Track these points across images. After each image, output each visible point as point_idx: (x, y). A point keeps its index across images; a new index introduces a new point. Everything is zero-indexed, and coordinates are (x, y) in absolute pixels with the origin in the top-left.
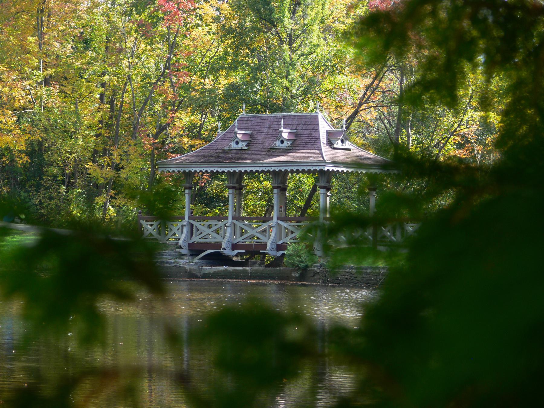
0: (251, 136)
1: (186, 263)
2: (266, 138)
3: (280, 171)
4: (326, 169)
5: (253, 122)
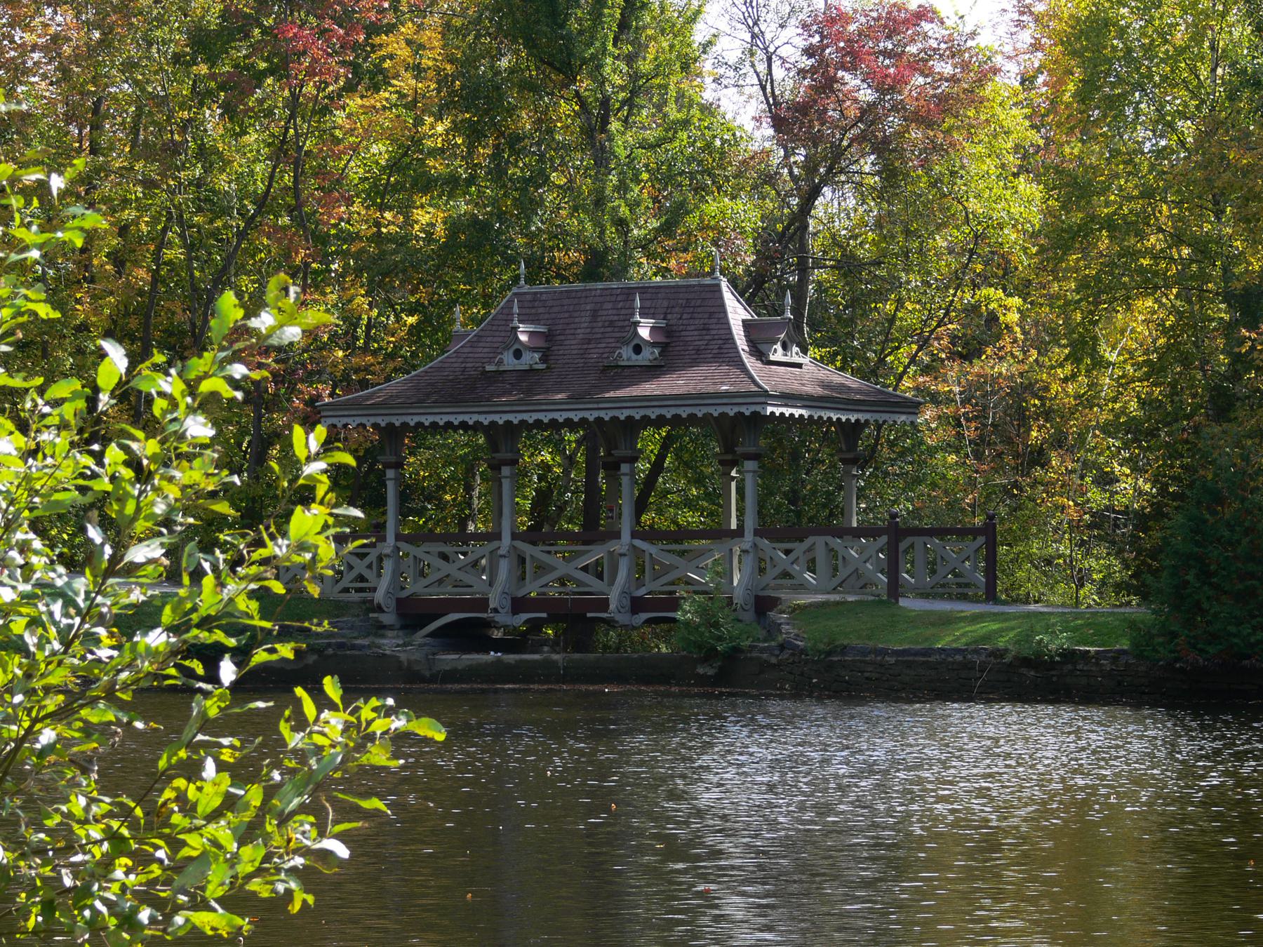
0: (548, 336)
1: (398, 646)
2: (589, 341)
3: (508, 423)
4: (769, 409)
5: (550, 303)
